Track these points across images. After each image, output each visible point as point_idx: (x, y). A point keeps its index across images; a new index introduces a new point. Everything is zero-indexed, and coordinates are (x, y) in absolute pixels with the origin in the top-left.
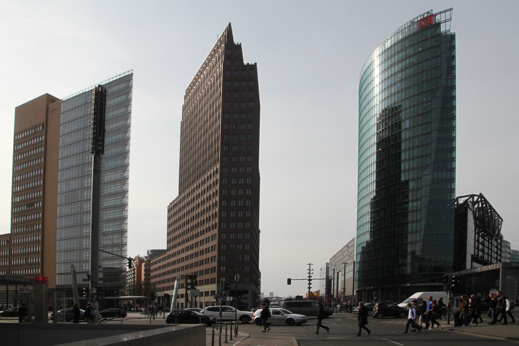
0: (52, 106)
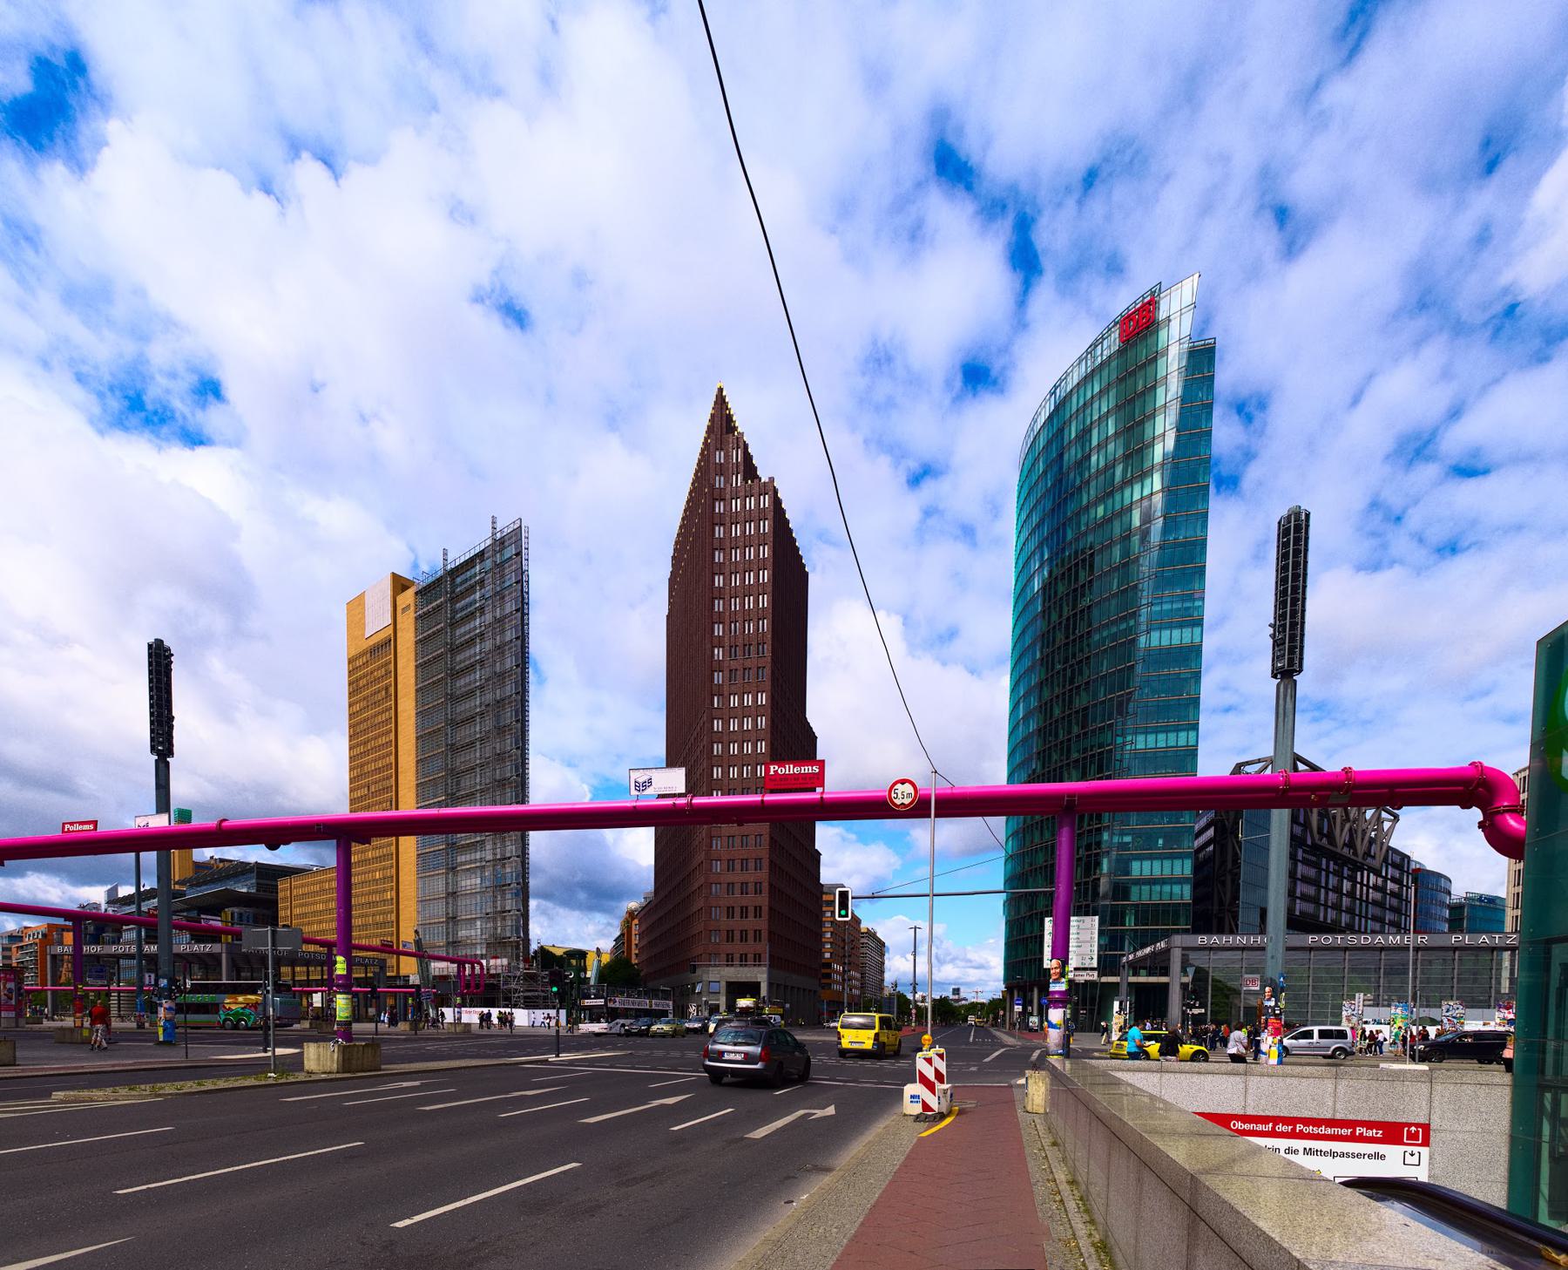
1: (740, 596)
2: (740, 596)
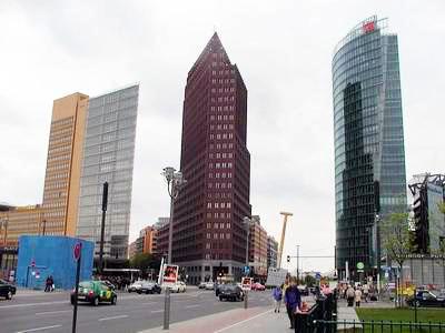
0: (81, 103)
1: (216, 99)
2: (216, 99)
